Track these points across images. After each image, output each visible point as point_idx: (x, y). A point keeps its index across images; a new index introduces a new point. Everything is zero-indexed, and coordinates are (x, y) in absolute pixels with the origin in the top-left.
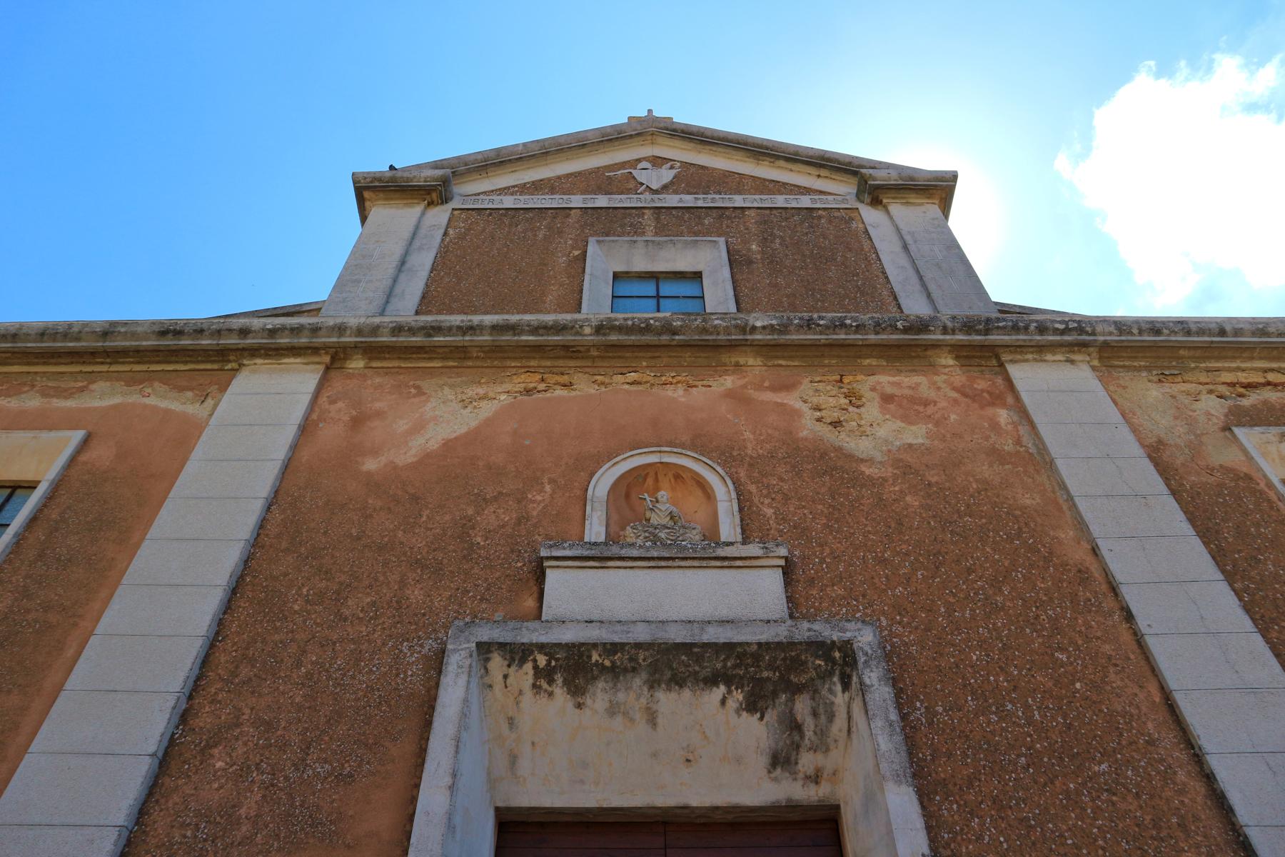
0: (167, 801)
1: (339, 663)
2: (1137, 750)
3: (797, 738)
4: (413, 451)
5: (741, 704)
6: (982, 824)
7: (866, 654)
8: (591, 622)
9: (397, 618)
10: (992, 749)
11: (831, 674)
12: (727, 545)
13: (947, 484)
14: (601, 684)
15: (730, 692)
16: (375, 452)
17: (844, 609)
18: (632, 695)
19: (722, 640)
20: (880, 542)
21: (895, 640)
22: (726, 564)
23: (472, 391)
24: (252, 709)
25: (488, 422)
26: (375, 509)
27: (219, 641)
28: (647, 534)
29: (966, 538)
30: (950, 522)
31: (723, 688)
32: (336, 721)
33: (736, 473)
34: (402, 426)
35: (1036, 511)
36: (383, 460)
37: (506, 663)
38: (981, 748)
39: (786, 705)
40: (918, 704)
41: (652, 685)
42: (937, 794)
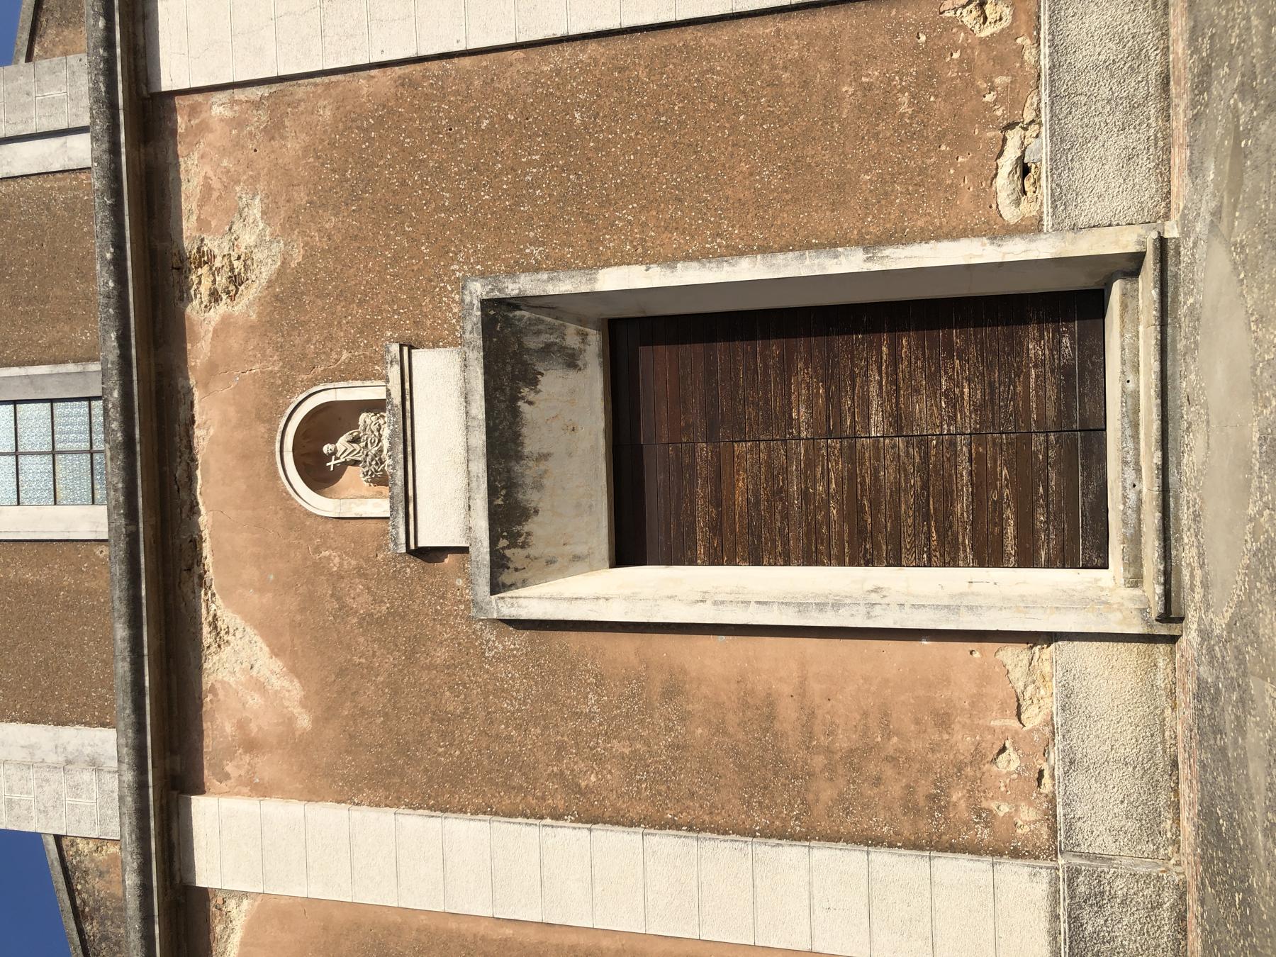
0: (622, 809)
1: (506, 705)
2: (564, 85)
3: (556, 348)
4: (286, 684)
5: (532, 389)
6: (620, 219)
7: (492, 290)
8: (469, 506)
9: (463, 666)
10: (563, 199)
11: (507, 318)
12: (390, 394)
13: (310, 186)
14: (520, 496)
15: (523, 398)
16: (290, 721)
17: (444, 299)
18: (528, 472)
19: (483, 403)
20: (375, 259)
21: (472, 261)
22: (408, 397)
23: (207, 637)
24: (548, 765)
25: (248, 618)
26: (355, 707)
27: (491, 810)
28: (374, 463)
29: (370, 180)
30: (353, 191)
31: (520, 403)
32: (555, 696)
33: (302, 382)
34: (255, 701)
35: (338, 109)
36: (297, 710)
37: (506, 570)
38: (563, 208)
39: (531, 355)
40: (528, 251)
41: (519, 457)
42: (598, 249)
